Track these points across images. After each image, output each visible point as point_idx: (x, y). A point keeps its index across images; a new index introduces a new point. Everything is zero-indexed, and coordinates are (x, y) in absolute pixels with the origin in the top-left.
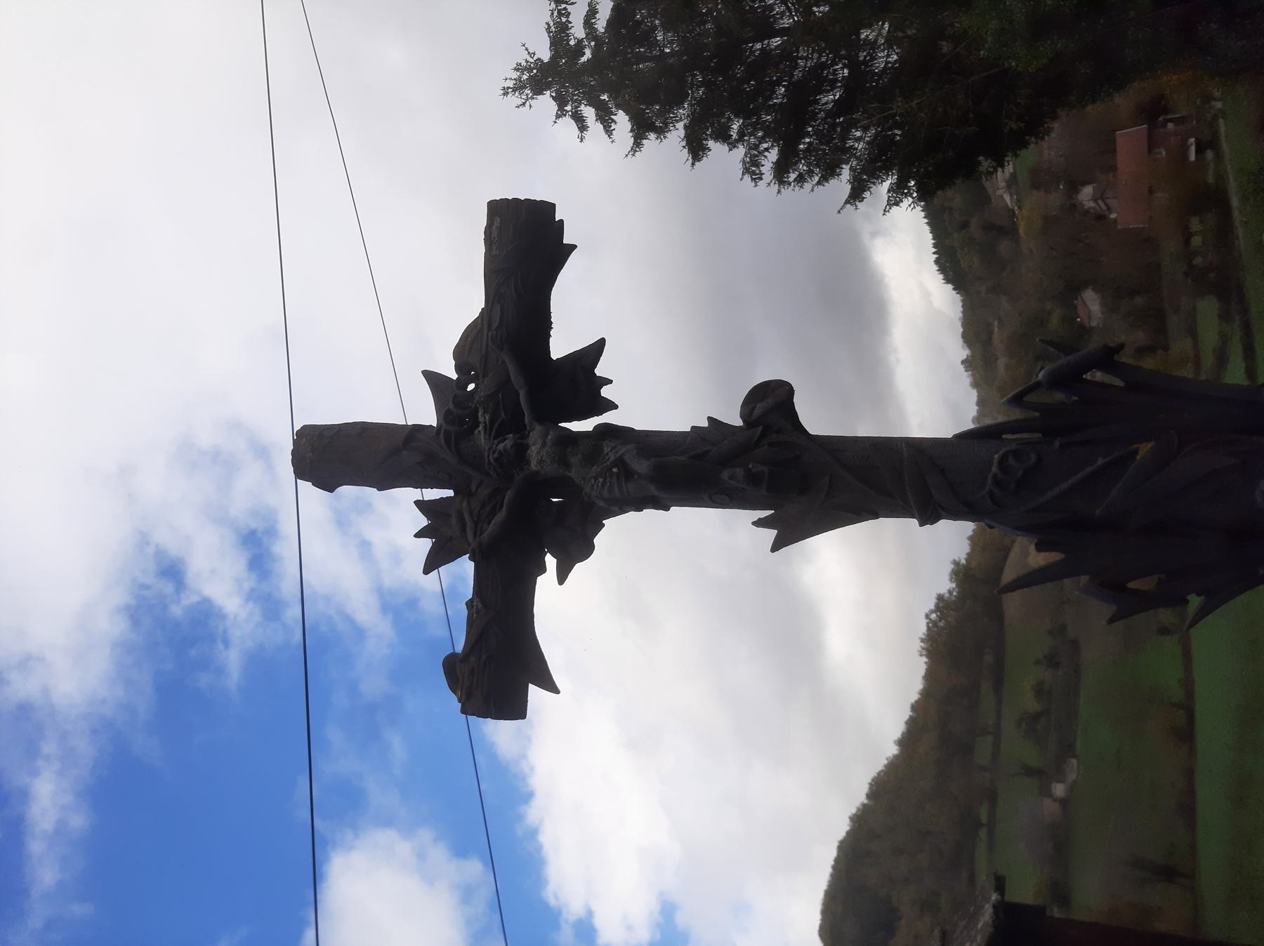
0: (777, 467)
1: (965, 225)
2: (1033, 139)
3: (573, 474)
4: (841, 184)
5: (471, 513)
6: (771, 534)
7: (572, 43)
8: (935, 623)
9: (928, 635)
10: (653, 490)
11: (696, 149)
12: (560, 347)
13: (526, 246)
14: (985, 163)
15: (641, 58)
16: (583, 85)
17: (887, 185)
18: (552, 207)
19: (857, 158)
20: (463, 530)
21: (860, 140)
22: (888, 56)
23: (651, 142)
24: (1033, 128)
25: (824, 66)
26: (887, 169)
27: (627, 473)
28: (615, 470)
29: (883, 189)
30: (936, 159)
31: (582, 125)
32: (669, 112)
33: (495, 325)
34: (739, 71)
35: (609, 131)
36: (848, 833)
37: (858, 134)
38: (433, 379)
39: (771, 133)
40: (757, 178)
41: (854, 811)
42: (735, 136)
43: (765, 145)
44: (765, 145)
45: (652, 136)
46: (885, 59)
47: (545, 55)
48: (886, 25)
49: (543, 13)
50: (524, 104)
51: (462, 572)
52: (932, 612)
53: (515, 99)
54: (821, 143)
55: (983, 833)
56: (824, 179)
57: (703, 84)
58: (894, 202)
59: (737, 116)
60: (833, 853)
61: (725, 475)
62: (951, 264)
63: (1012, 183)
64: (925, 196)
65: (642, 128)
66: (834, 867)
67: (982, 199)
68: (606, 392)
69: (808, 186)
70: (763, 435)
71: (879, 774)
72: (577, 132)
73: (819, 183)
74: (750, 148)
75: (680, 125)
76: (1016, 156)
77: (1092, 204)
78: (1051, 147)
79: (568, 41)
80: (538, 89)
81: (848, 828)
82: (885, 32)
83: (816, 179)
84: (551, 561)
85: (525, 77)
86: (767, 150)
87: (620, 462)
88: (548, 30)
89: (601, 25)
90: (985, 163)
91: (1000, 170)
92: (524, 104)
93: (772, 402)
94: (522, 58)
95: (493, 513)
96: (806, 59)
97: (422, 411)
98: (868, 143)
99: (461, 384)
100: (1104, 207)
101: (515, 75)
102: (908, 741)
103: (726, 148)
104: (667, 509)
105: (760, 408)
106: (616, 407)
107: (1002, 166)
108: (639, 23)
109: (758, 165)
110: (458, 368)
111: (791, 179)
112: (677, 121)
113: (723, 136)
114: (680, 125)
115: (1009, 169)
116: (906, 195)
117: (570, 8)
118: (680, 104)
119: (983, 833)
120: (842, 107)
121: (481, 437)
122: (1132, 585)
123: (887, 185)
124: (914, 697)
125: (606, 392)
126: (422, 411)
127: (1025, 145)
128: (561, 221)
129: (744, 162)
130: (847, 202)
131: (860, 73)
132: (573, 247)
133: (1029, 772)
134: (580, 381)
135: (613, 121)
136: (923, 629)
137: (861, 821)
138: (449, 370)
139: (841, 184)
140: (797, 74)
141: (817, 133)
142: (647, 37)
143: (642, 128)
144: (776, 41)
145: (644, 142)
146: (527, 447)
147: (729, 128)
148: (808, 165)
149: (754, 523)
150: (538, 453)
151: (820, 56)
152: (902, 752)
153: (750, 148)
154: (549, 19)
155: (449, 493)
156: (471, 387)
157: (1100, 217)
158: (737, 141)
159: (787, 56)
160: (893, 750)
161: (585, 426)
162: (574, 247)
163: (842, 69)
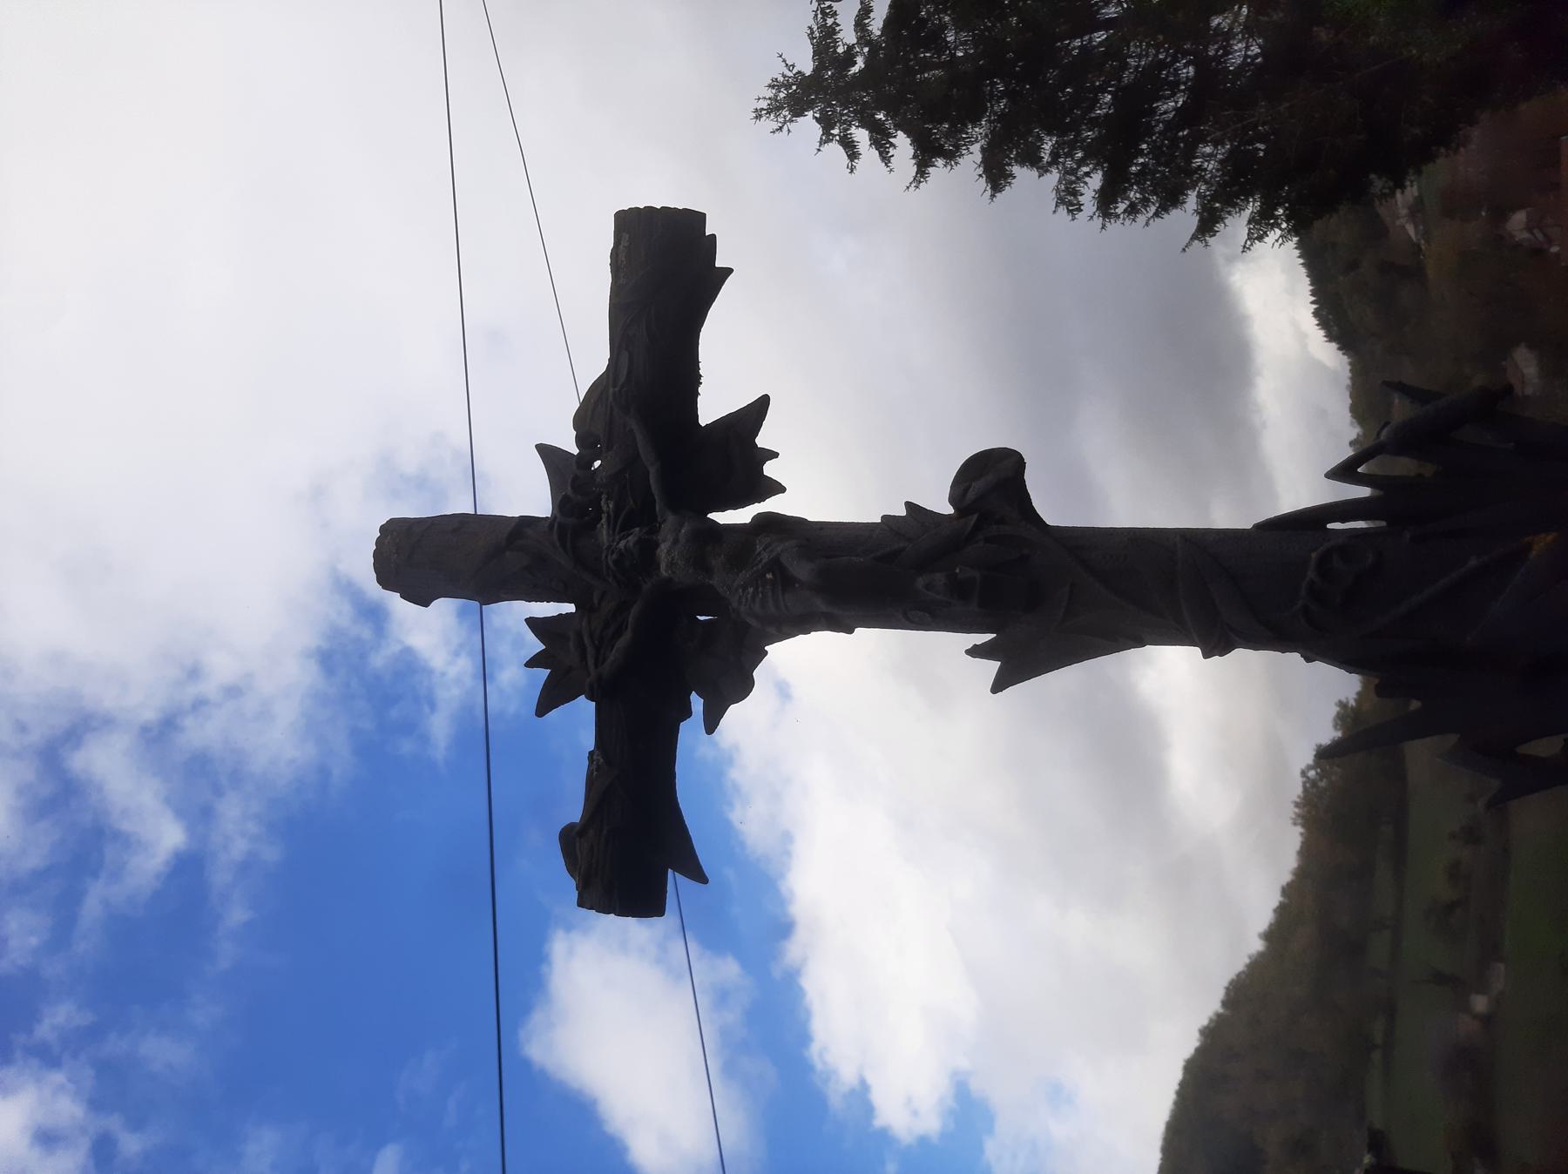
0: (1005, 575)
1: (1353, 266)
2: (1443, 150)
3: (715, 581)
4: (1185, 216)
5: (591, 636)
6: (993, 666)
7: (840, 50)
8: (1314, 783)
9: (1305, 798)
10: (821, 605)
11: (996, 176)
12: (712, 406)
13: (666, 271)
14: (1378, 184)
15: (927, 65)
16: (856, 102)
17: (1247, 213)
18: (700, 218)
19: (1206, 182)
20: (583, 657)
21: (1210, 158)
22: (1247, 48)
23: (938, 170)
24: (1441, 136)
25: (1162, 65)
26: (1248, 194)
27: (786, 582)
28: (769, 576)
29: (1237, 225)
30: (1310, 183)
31: (852, 151)
32: (962, 131)
33: (622, 379)
34: (1052, 75)
35: (886, 158)
36: (1197, 1050)
37: (1208, 150)
38: (548, 454)
39: (1094, 154)
40: (1074, 208)
41: (1205, 1022)
42: (1046, 158)
43: (1085, 169)
44: (1085, 169)
45: (940, 162)
46: (1244, 51)
47: (807, 66)
48: (1245, 10)
49: (805, 16)
50: (781, 129)
51: (579, 720)
52: (1310, 768)
53: (769, 123)
54: (1159, 164)
55: (1376, 1056)
56: (1164, 208)
57: (1003, 94)
58: (1256, 236)
59: (1049, 134)
60: (1178, 1075)
61: (920, 582)
62: (1334, 315)
63: (1416, 210)
64: (1300, 227)
65: (927, 154)
66: (1180, 1094)
67: (1377, 231)
68: (770, 469)
69: (1141, 219)
70: (977, 528)
71: (1238, 975)
72: (846, 160)
73: (1157, 214)
74: (1067, 173)
75: (976, 148)
76: (1419, 172)
77: (1526, 235)
78: (1467, 162)
79: (835, 47)
80: (798, 112)
81: (1197, 1044)
82: (1242, 19)
83: (1153, 209)
84: (697, 703)
85: (782, 95)
86: (1087, 174)
87: (776, 565)
88: (811, 36)
89: (876, 25)
90: (1378, 184)
91: (1398, 192)
92: (781, 129)
93: (993, 481)
94: (778, 71)
95: (618, 633)
96: (1137, 58)
97: (528, 495)
98: (1221, 162)
99: (583, 461)
100: (1540, 236)
101: (770, 93)
102: (1276, 935)
103: (1035, 173)
104: (850, 631)
105: (977, 487)
106: (783, 490)
107: (1402, 187)
108: (923, 22)
109: (1075, 193)
110: (579, 441)
111: (1119, 211)
112: (972, 143)
113: (1031, 159)
114: (976, 148)
115: (1412, 191)
116: (1272, 226)
117: (836, 6)
118: (975, 121)
119: (1376, 1056)
120: (1185, 116)
121: (604, 533)
122: (1524, 749)
123: (1247, 213)
124: (1287, 878)
125: (770, 469)
126: (528, 495)
127: (1430, 157)
128: (713, 237)
129: (1058, 190)
130: (1194, 237)
131: (1210, 72)
132: (729, 271)
133: (1440, 978)
134: (736, 455)
135: (892, 145)
136: (1299, 790)
137: (1213, 1035)
138: (568, 442)
139: (1185, 216)
140: (1127, 77)
141: (1155, 151)
142: (935, 40)
143: (927, 154)
144: (1100, 36)
145: (930, 170)
146: (657, 545)
147: (1039, 148)
148: (1142, 191)
149: (969, 652)
150: (669, 550)
151: (1158, 53)
152: (1268, 948)
153: (1067, 173)
154: (812, 23)
155: (570, 608)
156: (597, 464)
157: (1538, 252)
158: (1050, 164)
159: (1114, 51)
160: (1258, 946)
161: (741, 516)
162: (730, 271)
163: (1186, 66)
